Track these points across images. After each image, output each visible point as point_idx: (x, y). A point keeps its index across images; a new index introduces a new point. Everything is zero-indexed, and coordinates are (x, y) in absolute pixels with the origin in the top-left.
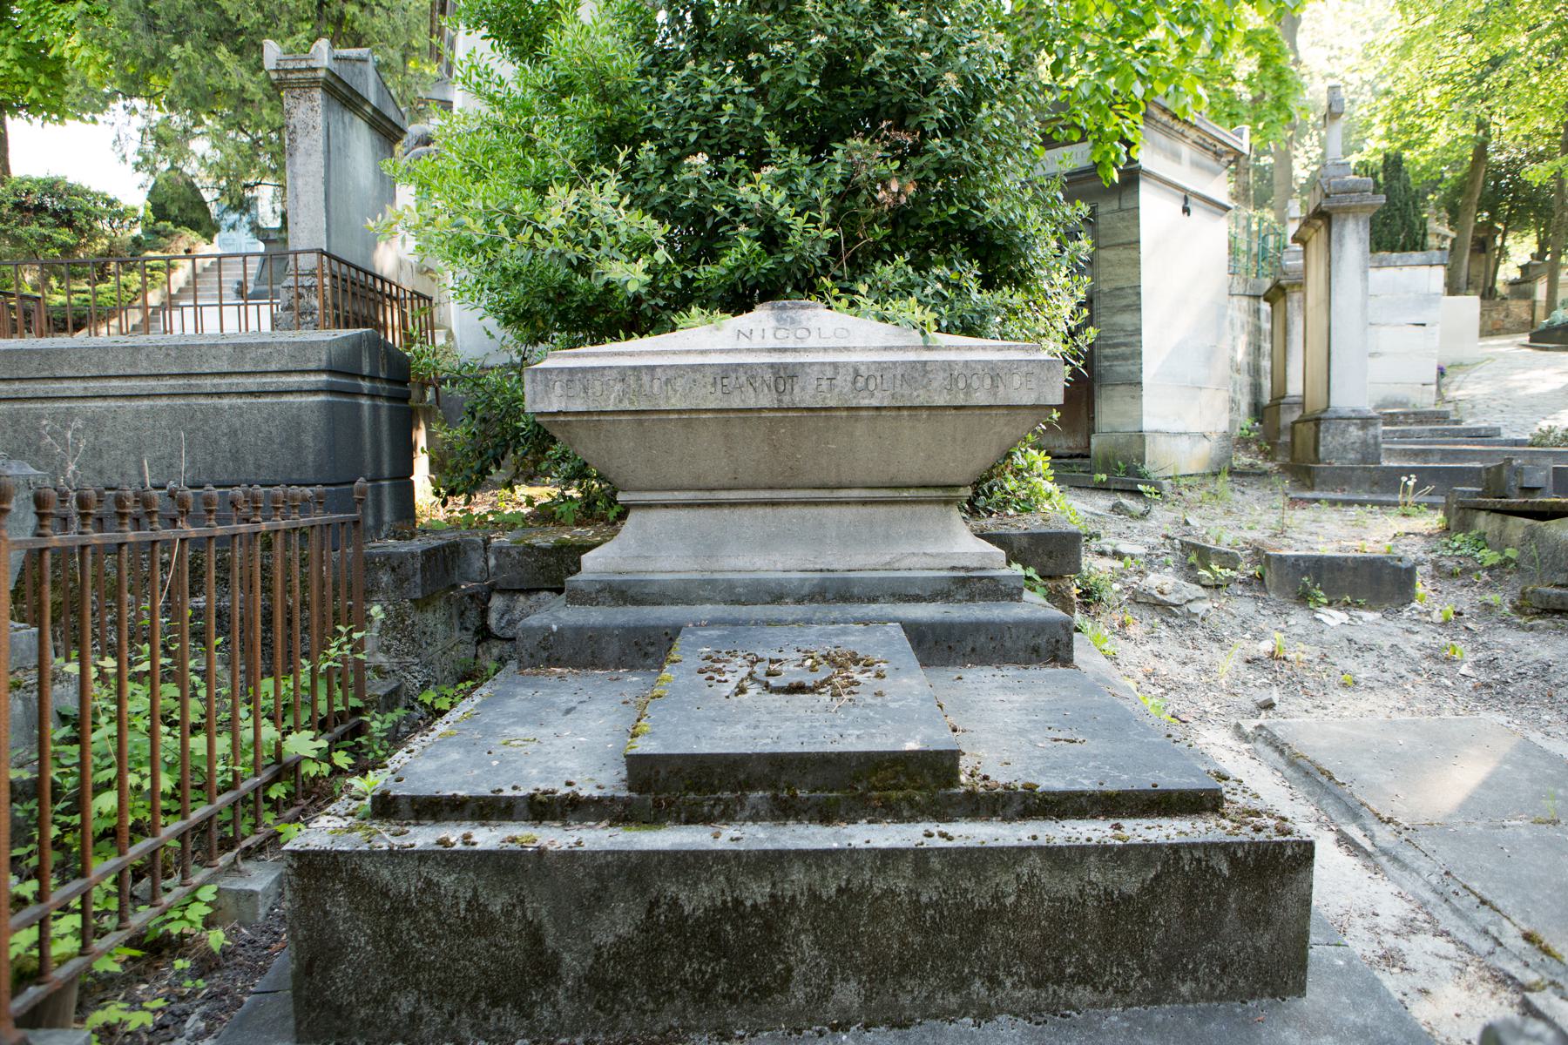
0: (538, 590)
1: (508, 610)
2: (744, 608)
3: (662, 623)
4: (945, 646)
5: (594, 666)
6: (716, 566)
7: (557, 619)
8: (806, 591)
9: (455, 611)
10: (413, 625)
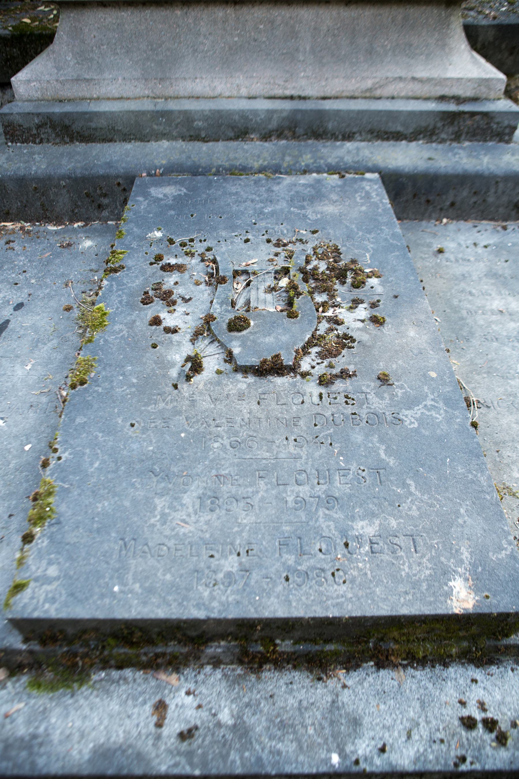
2: (205, 147)
3: (113, 172)
4: (423, 199)
6: (170, 92)
8: (274, 124)
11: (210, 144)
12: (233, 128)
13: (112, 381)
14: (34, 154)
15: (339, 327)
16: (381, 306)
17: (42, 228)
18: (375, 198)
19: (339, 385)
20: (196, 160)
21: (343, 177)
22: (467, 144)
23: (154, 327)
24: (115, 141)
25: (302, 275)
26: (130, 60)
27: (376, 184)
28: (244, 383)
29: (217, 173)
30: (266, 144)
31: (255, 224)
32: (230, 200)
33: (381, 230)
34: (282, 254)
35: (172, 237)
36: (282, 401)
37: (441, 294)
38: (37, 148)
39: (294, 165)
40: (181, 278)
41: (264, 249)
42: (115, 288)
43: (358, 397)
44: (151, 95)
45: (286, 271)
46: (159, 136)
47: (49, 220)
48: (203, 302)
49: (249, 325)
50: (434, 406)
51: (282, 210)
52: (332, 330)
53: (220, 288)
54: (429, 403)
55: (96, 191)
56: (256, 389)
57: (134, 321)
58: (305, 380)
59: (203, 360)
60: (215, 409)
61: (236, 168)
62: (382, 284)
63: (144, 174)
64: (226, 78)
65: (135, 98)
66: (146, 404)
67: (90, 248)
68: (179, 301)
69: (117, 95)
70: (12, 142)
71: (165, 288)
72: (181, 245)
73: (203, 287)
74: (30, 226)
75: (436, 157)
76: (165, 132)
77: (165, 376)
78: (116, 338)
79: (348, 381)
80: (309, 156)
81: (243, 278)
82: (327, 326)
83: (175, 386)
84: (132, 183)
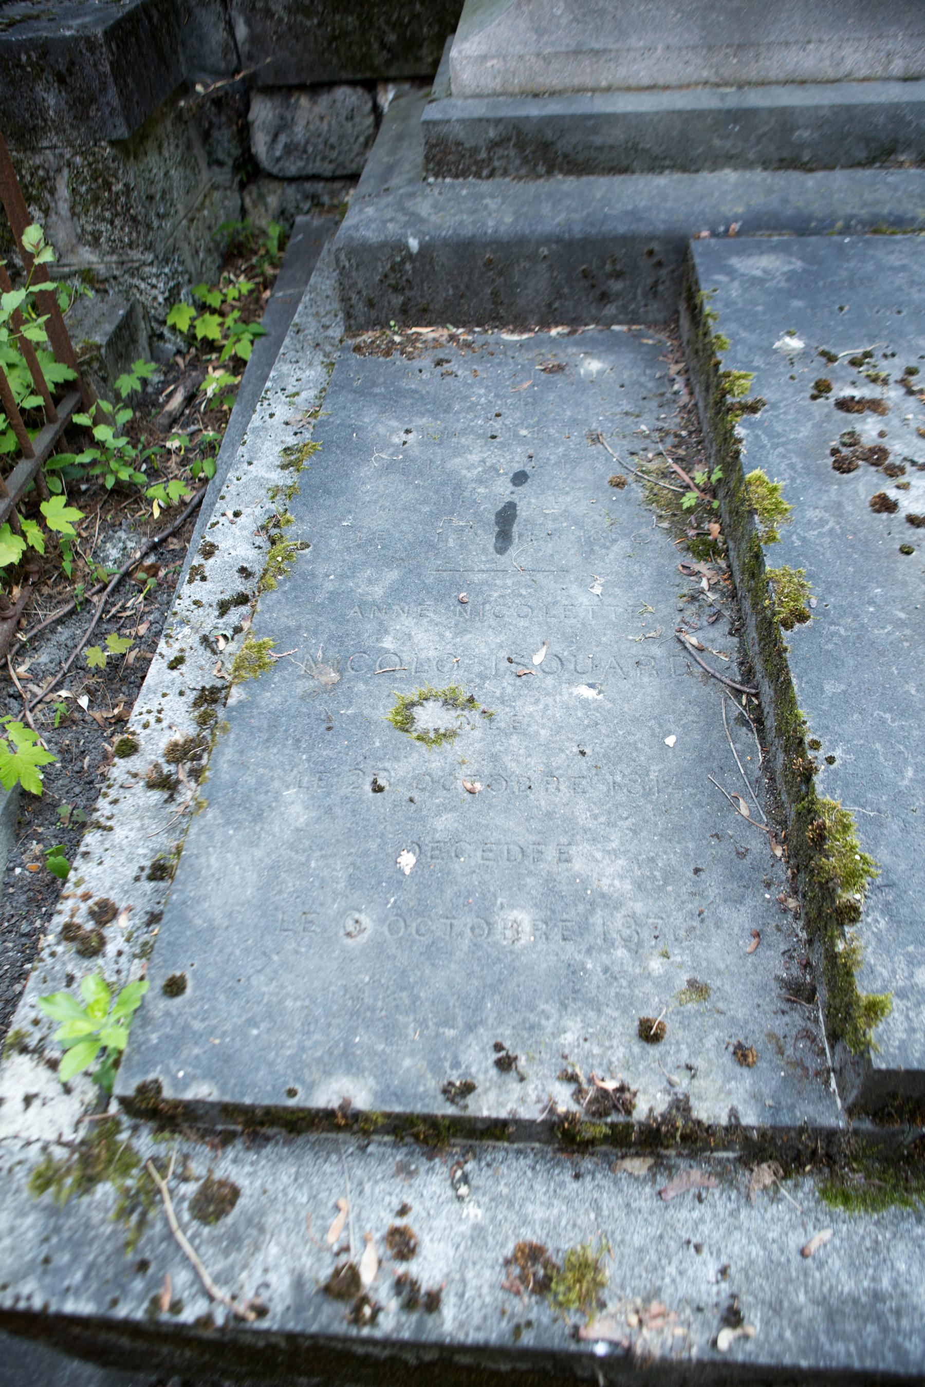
0: (330, 85)
1: (283, 126)
2: (812, 181)
3: (643, 228)
5: (498, 320)
6: (752, 72)
7: (415, 220)
9: (193, 132)
10: (128, 190)
11: (820, 175)
12: (867, 141)
20: (801, 204)
24: (633, 172)
26: (678, 11)
29: (846, 230)
38: (485, 186)
40: (887, 424)
42: (765, 440)
44: (713, 79)
46: (718, 160)
64: (870, 38)
65: (681, 87)
67: (601, 373)
69: (646, 81)
70: (436, 176)
76: (733, 152)
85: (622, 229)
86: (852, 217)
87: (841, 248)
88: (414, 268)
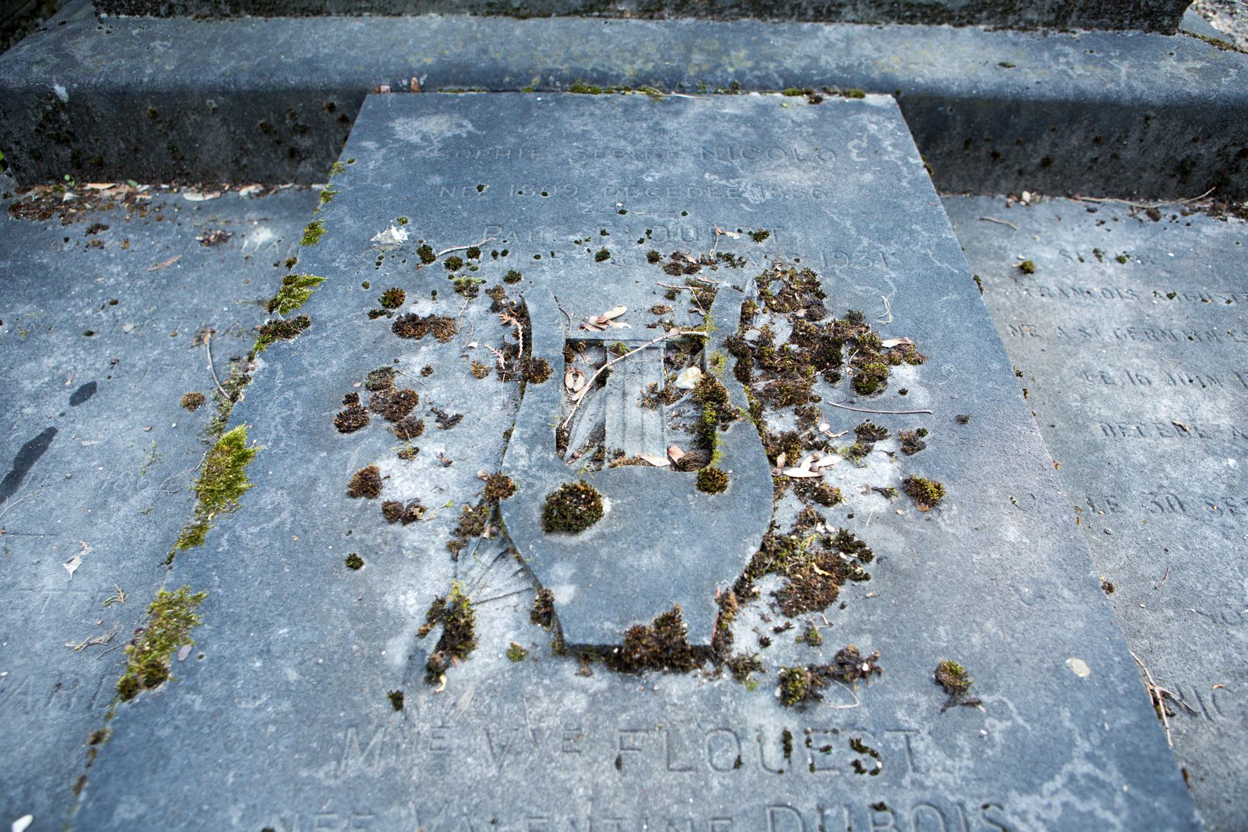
2: (518, 29)
3: (317, 81)
13: (233, 676)
14: (153, 39)
15: (827, 512)
16: (929, 448)
17: (172, 198)
18: (892, 155)
19: (837, 705)
20: (498, 56)
21: (818, 100)
22: (1080, 33)
23: (361, 501)
24: (329, 14)
25: (733, 361)
27: (890, 119)
28: (582, 689)
30: (651, 25)
31: (622, 212)
32: (568, 151)
33: (911, 232)
34: (685, 292)
35: (430, 242)
36: (683, 759)
37: (1039, 380)
38: (162, 25)
39: (711, 72)
40: (441, 356)
41: (642, 279)
43: (886, 746)
45: (694, 345)
47: (188, 180)
48: (487, 426)
49: (598, 510)
50: (1095, 779)
51: (684, 178)
52: (812, 522)
53: (534, 391)
54: (1083, 768)
55: (283, 122)
56: (612, 716)
57: (314, 481)
58: (744, 686)
59: (479, 611)
60: (497, 780)
61: (584, 77)
62: (927, 382)
63: (385, 88)
66: (315, 760)
67: (266, 245)
68: (430, 423)
70: (109, 12)
71: (399, 383)
72: (448, 266)
73: (491, 382)
74: (149, 192)
75: (1017, 62)
77: (374, 661)
78: (260, 535)
79: (859, 689)
80: (743, 53)
81: (590, 358)
82: (798, 506)
83: (397, 700)
84: (359, 104)
85: (293, 81)
86: (551, 71)
87: (527, 107)
88: (71, 119)
